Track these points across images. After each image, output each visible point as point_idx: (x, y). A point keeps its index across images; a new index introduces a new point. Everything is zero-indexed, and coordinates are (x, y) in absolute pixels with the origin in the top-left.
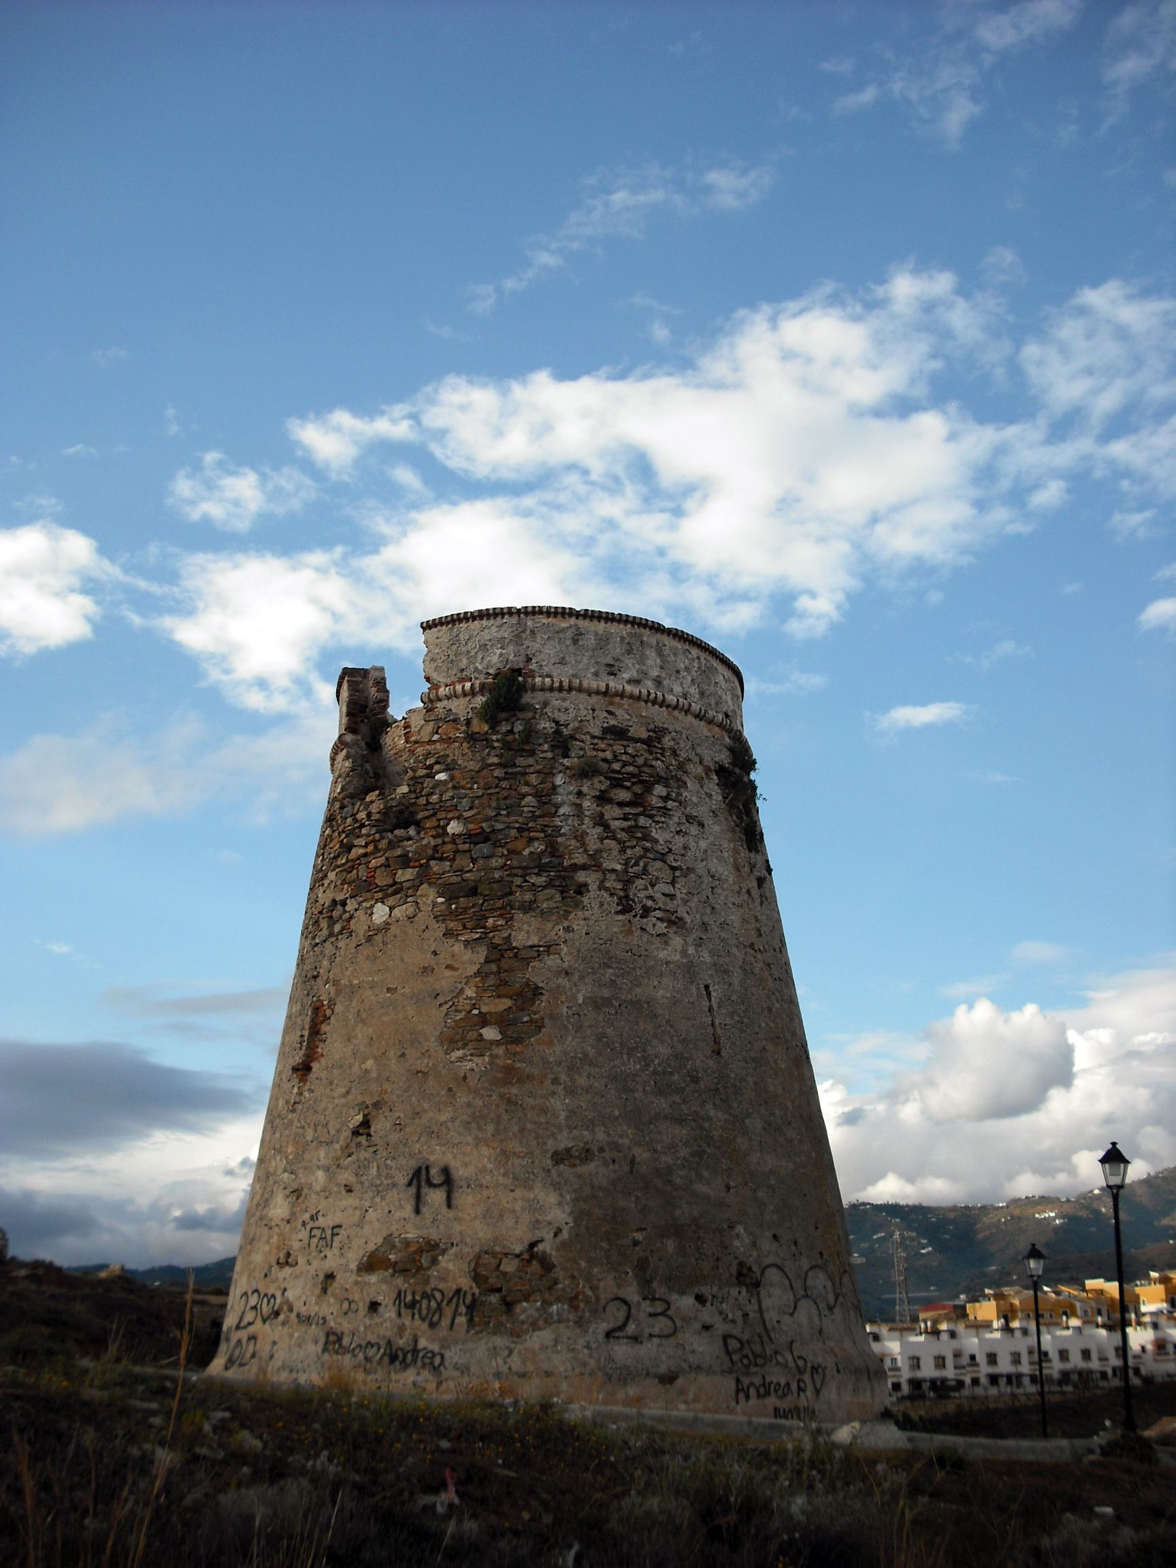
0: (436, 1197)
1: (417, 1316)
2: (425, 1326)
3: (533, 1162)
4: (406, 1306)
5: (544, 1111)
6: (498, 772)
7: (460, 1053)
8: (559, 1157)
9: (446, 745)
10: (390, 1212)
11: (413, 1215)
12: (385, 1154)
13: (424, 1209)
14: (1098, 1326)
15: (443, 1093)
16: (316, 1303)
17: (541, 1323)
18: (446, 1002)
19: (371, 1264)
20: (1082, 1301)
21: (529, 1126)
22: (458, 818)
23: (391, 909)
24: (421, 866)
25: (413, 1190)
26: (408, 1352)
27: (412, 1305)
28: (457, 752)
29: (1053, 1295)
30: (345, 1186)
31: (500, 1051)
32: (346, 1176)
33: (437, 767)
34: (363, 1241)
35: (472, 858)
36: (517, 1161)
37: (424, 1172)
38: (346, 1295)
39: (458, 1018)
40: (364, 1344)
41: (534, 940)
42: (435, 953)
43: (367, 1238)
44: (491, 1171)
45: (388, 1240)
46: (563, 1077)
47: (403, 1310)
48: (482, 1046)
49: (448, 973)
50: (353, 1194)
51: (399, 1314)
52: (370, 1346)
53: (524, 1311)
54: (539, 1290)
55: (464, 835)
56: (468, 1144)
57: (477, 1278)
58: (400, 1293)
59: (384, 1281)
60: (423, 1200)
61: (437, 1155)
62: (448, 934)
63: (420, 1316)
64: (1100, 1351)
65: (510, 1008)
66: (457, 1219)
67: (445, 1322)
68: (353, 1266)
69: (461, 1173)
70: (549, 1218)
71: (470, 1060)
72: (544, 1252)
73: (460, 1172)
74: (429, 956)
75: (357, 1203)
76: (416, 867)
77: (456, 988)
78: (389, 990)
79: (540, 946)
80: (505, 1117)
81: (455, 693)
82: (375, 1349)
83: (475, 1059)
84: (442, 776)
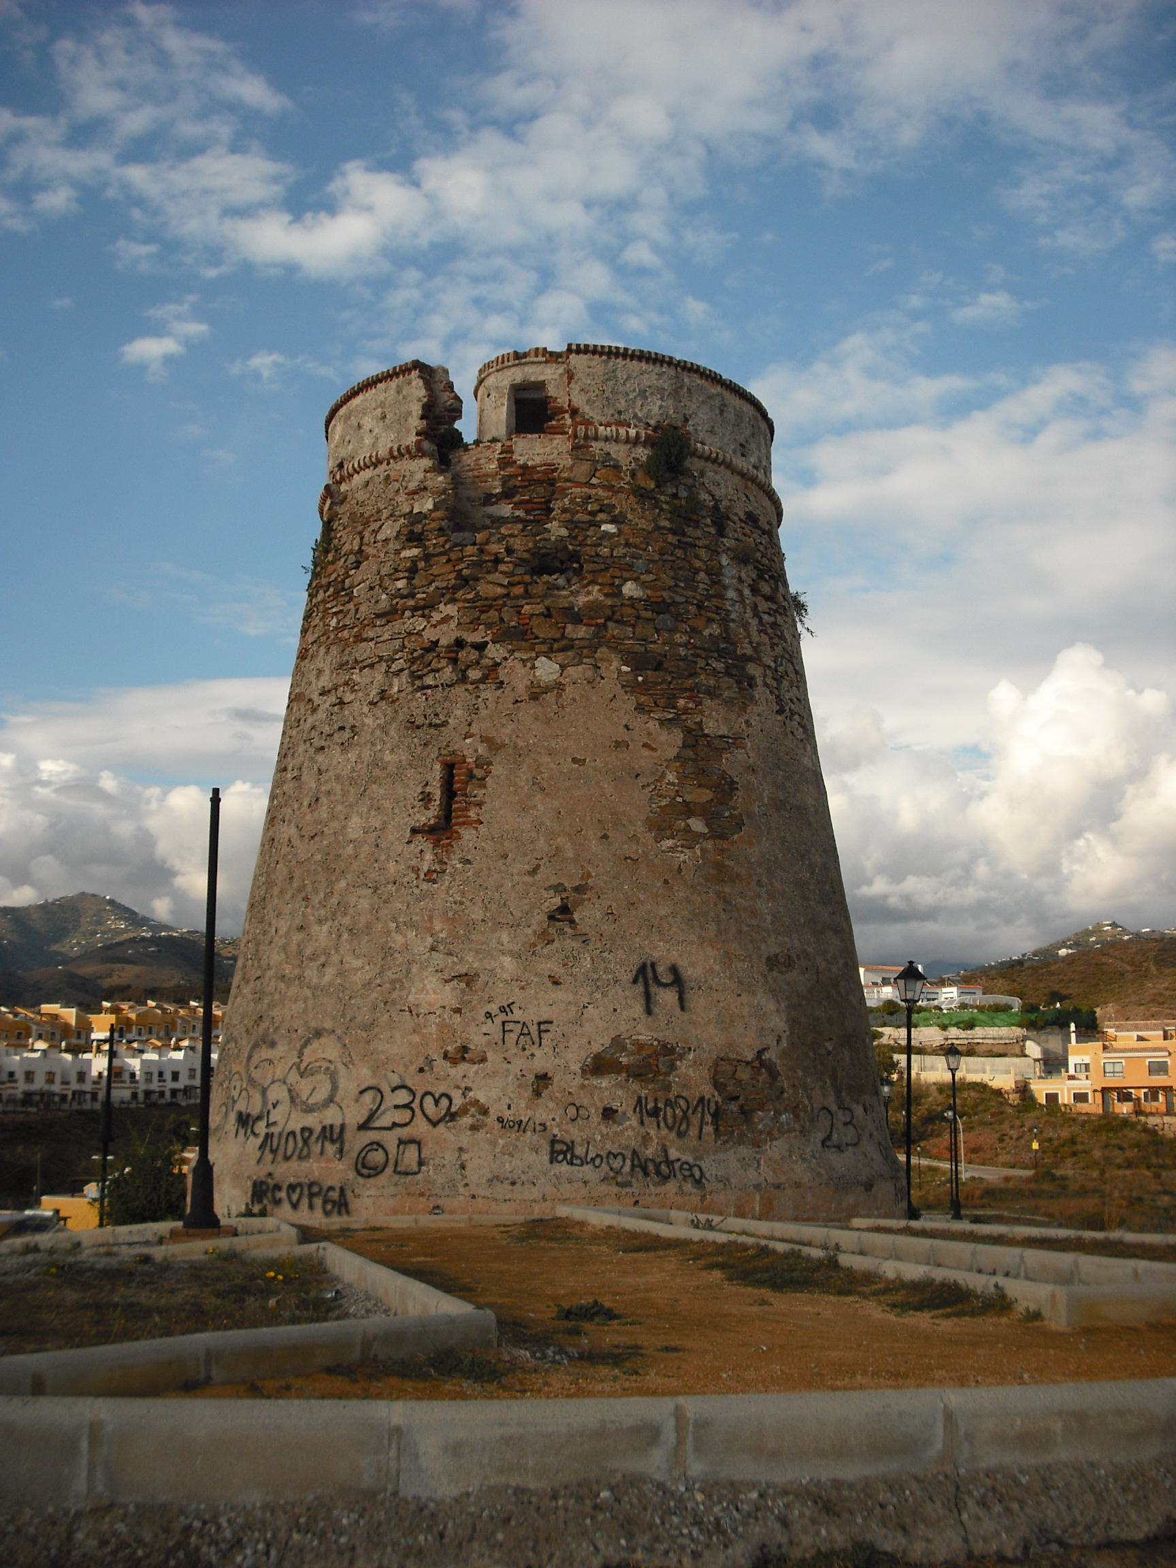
0: (667, 997)
1: (662, 1124)
2: (673, 1136)
3: (752, 967)
4: (649, 1114)
5: (754, 913)
6: (671, 538)
7: (670, 843)
8: (772, 962)
9: (610, 494)
10: (615, 1010)
11: (644, 1016)
12: (599, 945)
13: (656, 1010)
14: (61, 1051)
15: (659, 884)
16: (527, 1107)
17: (775, 1133)
18: (648, 785)
19: (599, 1066)
20: (38, 1023)
21: (745, 929)
22: (636, 580)
23: (563, 667)
24: (597, 625)
25: (640, 988)
26: (660, 1163)
27: (655, 1113)
28: (624, 503)
29: (11, 1016)
30: (549, 976)
31: (709, 845)
32: (551, 966)
33: (601, 516)
34: (586, 1040)
35: (656, 628)
36: (739, 965)
37: (649, 969)
38: (570, 1100)
39: (663, 803)
40: (603, 1154)
41: (724, 731)
42: (627, 727)
43: (590, 1037)
44: (719, 974)
45: (618, 1043)
46: (765, 880)
47: (645, 1118)
48: (691, 839)
49: (646, 752)
50: (562, 986)
51: (642, 1123)
52: (612, 1157)
53: (761, 1120)
54: (772, 1100)
55: (644, 601)
56: (692, 943)
57: (717, 1085)
58: (639, 1100)
59: (619, 1085)
60: (653, 1000)
61: (663, 953)
62: (640, 708)
63: (666, 1123)
64: (64, 1075)
65: (712, 800)
66: (691, 1022)
67: (693, 1132)
68: (576, 1067)
69: (689, 973)
70: (771, 1025)
71: (682, 852)
72: (770, 1059)
73: (690, 973)
74: (622, 730)
75: (571, 997)
76: (592, 625)
77: (657, 770)
78: (575, 760)
79: (729, 737)
80: (723, 916)
81: (617, 437)
82: (619, 1159)
83: (686, 851)
84: (610, 528)
